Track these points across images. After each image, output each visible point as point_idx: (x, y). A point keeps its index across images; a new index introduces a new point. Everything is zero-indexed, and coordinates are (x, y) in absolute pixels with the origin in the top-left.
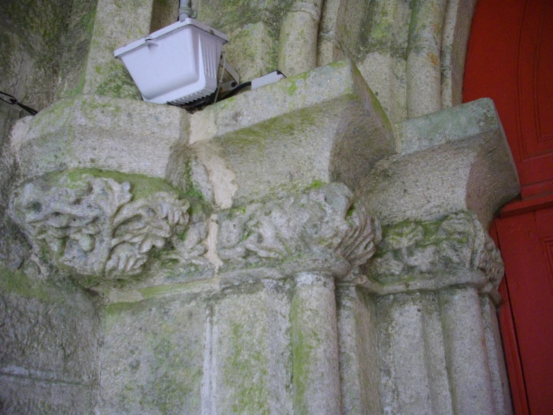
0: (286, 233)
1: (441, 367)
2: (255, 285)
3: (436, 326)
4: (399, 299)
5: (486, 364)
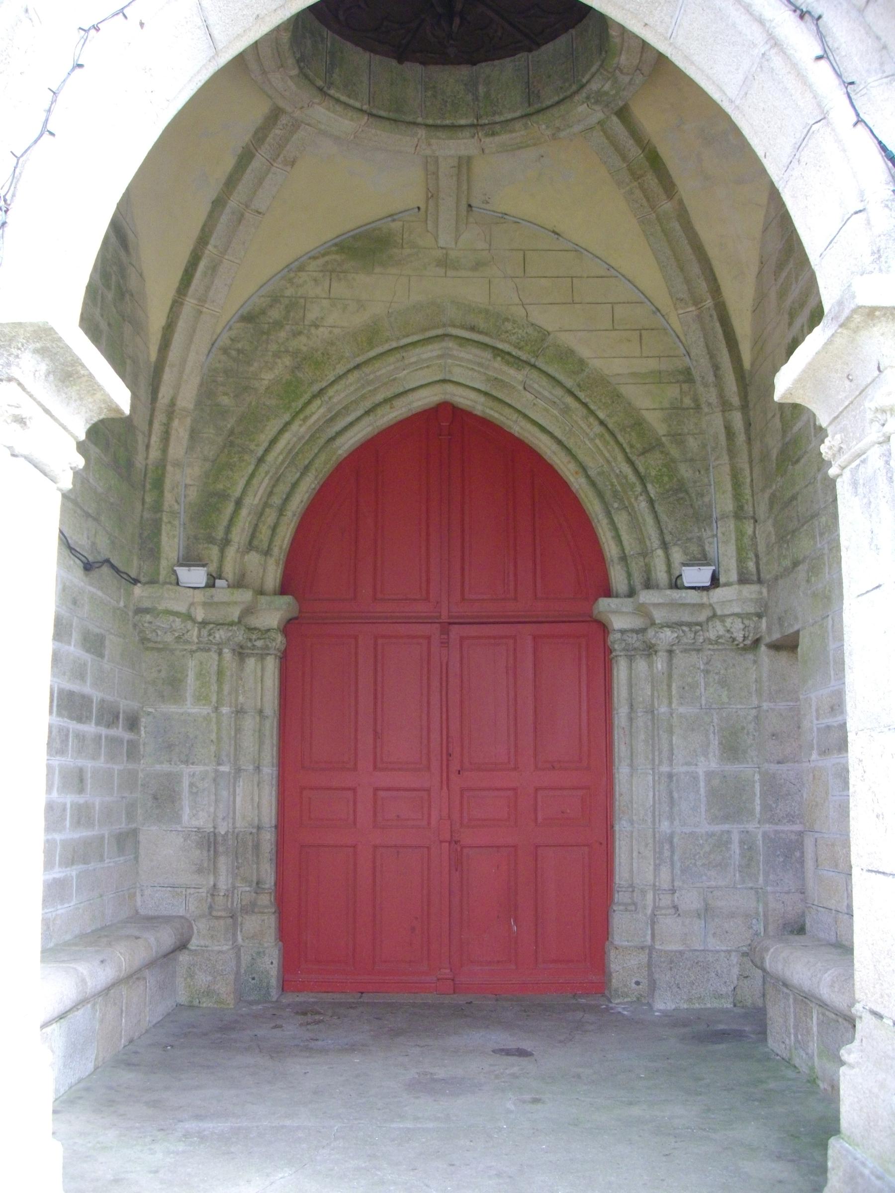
0: (223, 637)
1: (259, 680)
2: (209, 650)
3: (259, 666)
4: (249, 656)
5: (274, 681)
